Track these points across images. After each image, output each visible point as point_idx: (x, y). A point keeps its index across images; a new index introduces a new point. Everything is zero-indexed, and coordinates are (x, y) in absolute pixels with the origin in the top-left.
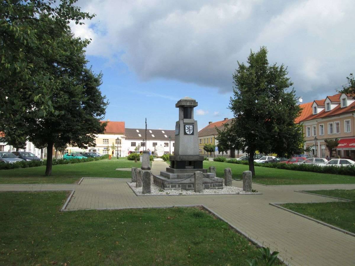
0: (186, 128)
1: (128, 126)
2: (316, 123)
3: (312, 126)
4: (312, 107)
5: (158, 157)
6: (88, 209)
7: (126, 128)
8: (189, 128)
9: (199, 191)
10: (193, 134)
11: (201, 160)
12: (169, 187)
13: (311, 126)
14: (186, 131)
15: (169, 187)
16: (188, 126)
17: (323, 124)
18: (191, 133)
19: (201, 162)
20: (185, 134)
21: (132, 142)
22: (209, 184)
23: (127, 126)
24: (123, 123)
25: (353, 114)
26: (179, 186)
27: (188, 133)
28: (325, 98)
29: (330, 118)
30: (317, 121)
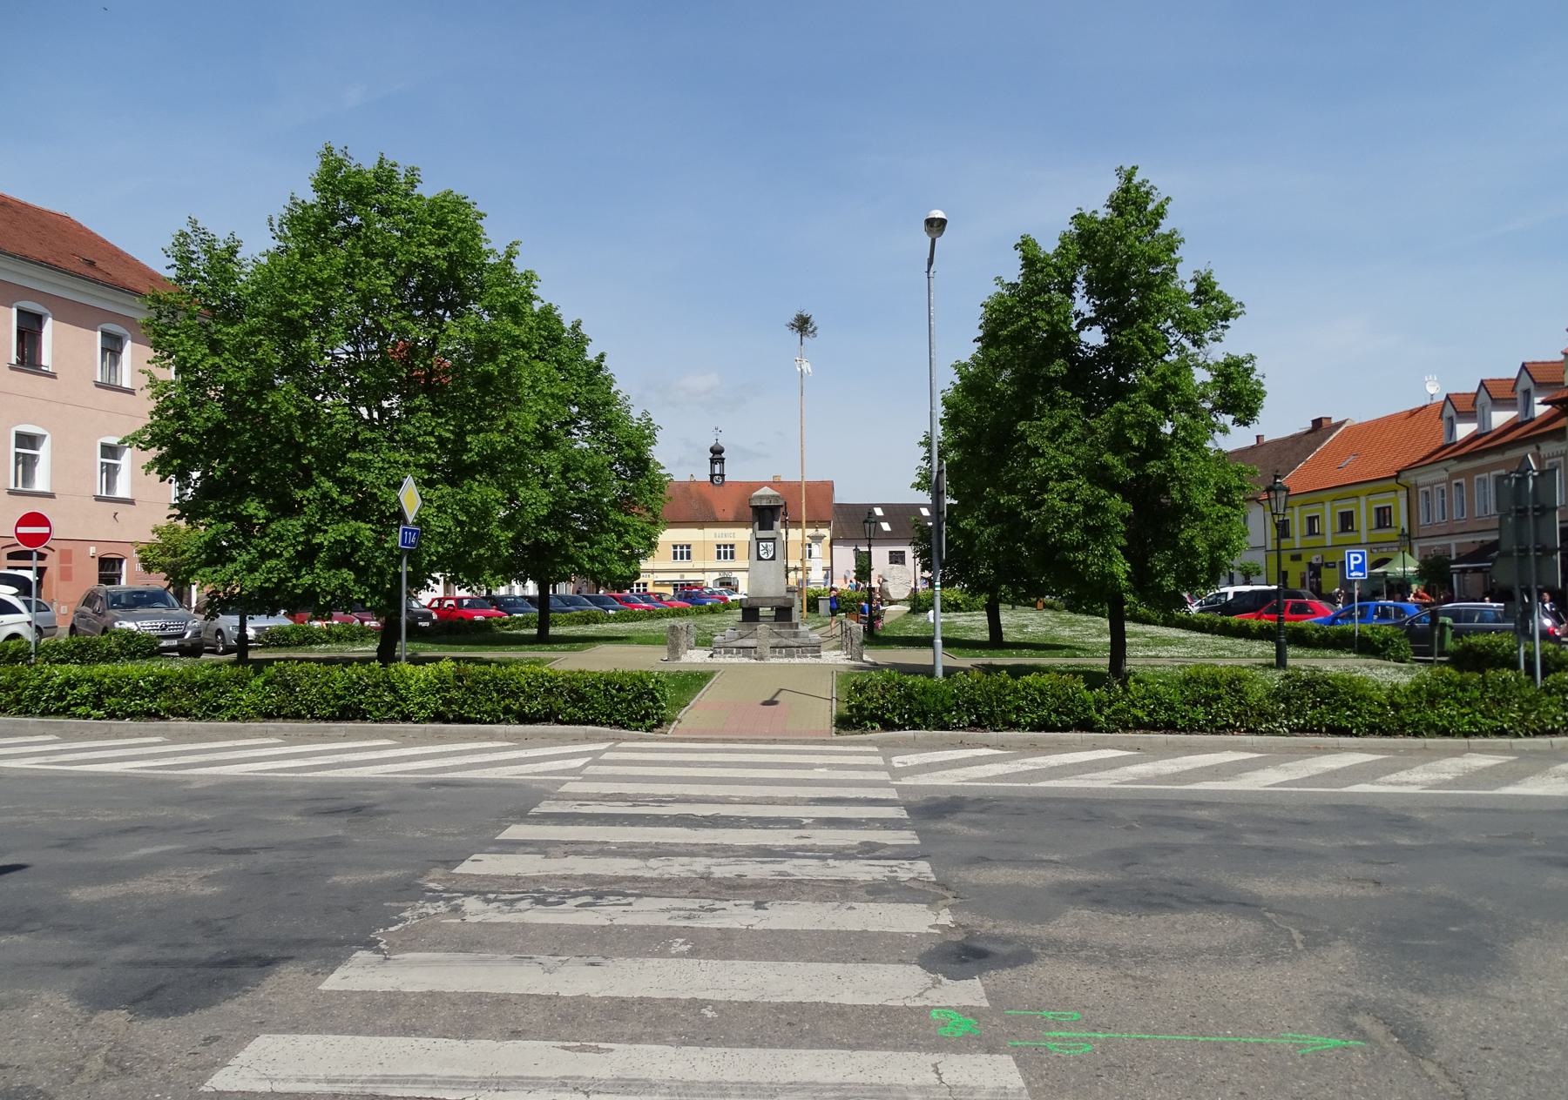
0: (761, 548)
1: (845, 495)
2: (1445, 475)
3: (1436, 486)
4: (1441, 417)
5: (892, 603)
6: (793, 902)
7: (837, 501)
8: (766, 548)
9: (762, 658)
10: (773, 558)
11: (787, 606)
12: (720, 653)
13: (1432, 485)
14: (761, 553)
15: (720, 653)
16: (764, 544)
17: (1462, 480)
18: (770, 556)
19: (758, 609)
20: (760, 558)
21: (891, 552)
22: (795, 650)
23: (842, 496)
24: (828, 487)
25: (1538, 448)
26: (738, 653)
27: (764, 557)
28: (1475, 390)
29: (1480, 458)
30: (1447, 470)
